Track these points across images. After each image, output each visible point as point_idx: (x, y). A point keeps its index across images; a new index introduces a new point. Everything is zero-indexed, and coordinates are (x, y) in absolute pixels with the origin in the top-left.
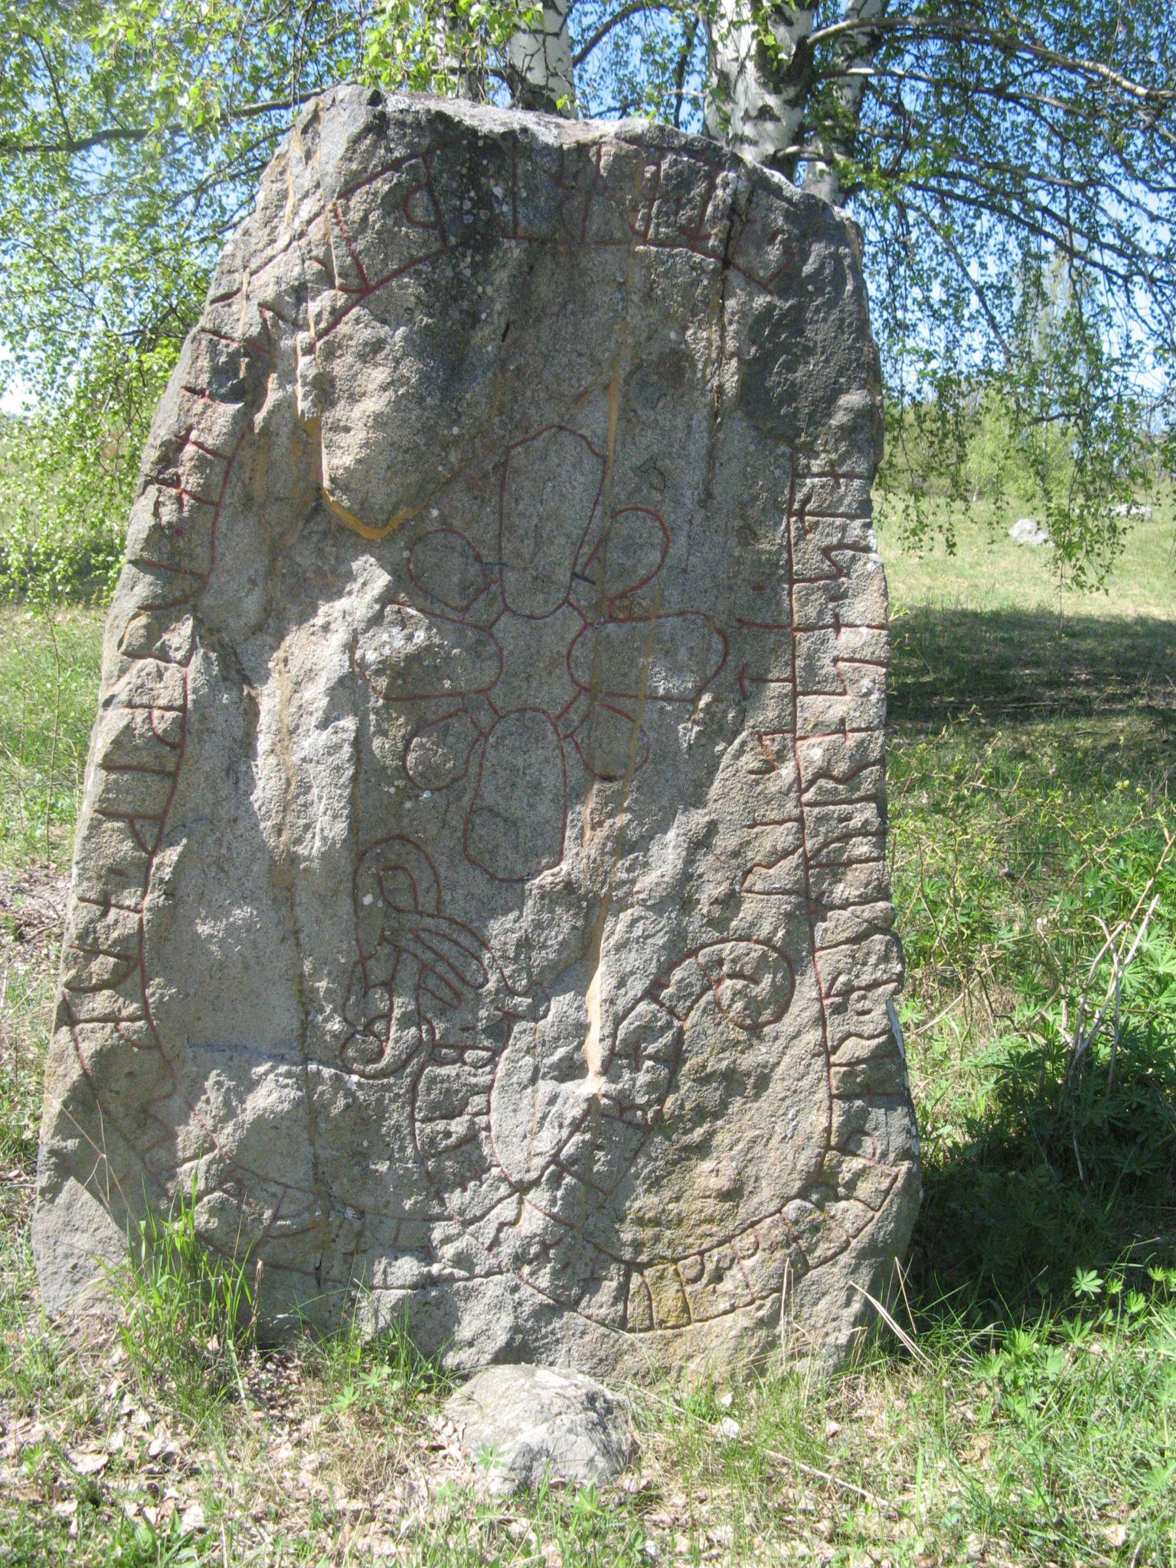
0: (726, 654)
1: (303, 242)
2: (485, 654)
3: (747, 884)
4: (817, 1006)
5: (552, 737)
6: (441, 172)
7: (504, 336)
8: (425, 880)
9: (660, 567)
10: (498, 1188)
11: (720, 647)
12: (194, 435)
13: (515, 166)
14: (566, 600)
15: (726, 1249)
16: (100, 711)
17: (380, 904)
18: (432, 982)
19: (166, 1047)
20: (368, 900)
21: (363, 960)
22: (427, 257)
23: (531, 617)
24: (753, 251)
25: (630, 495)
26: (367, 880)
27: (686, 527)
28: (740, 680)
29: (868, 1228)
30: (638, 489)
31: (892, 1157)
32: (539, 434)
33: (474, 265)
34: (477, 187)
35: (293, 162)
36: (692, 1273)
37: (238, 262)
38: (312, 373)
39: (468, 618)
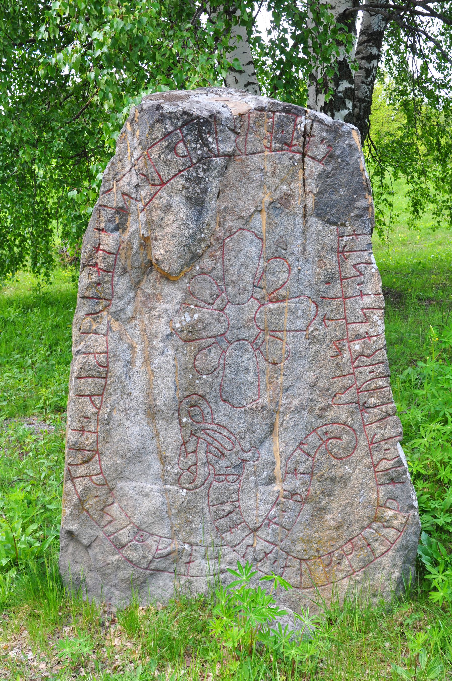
0: (317, 311)
1: (136, 167)
2: (222, 320)
3: (334, 401)
4: (368, 448)
5: (251, 350)
6: (187, 134)
7: (218, 196)
8: (207, 410)
9: (288, 279)
10: (244, 531)
11: (315, 308)
12: (101, 247)
13: (216, 128)
14: (252, 296)
15: (340, 551)
16: (74, 357)
17: (189, 421)
18: (212, 449)
19: (110, 484)
20: (184, 420)
21: (184, 443)
22: (185, 169)
23: (239, 304)
24: (314, 148)
25: (273, 253)
26: (183, 412)
27: (297, 263)
28: (324, 320)
29: (399, 540)
30: (276, 250)
31: (406, 509)
32: (235, 232)
33: (204, 171)
34: (202, 138)
35: (128, 135)
36: (327, 562)
37: (111, 176)
38: (145, 219)
39: (215, 307)
